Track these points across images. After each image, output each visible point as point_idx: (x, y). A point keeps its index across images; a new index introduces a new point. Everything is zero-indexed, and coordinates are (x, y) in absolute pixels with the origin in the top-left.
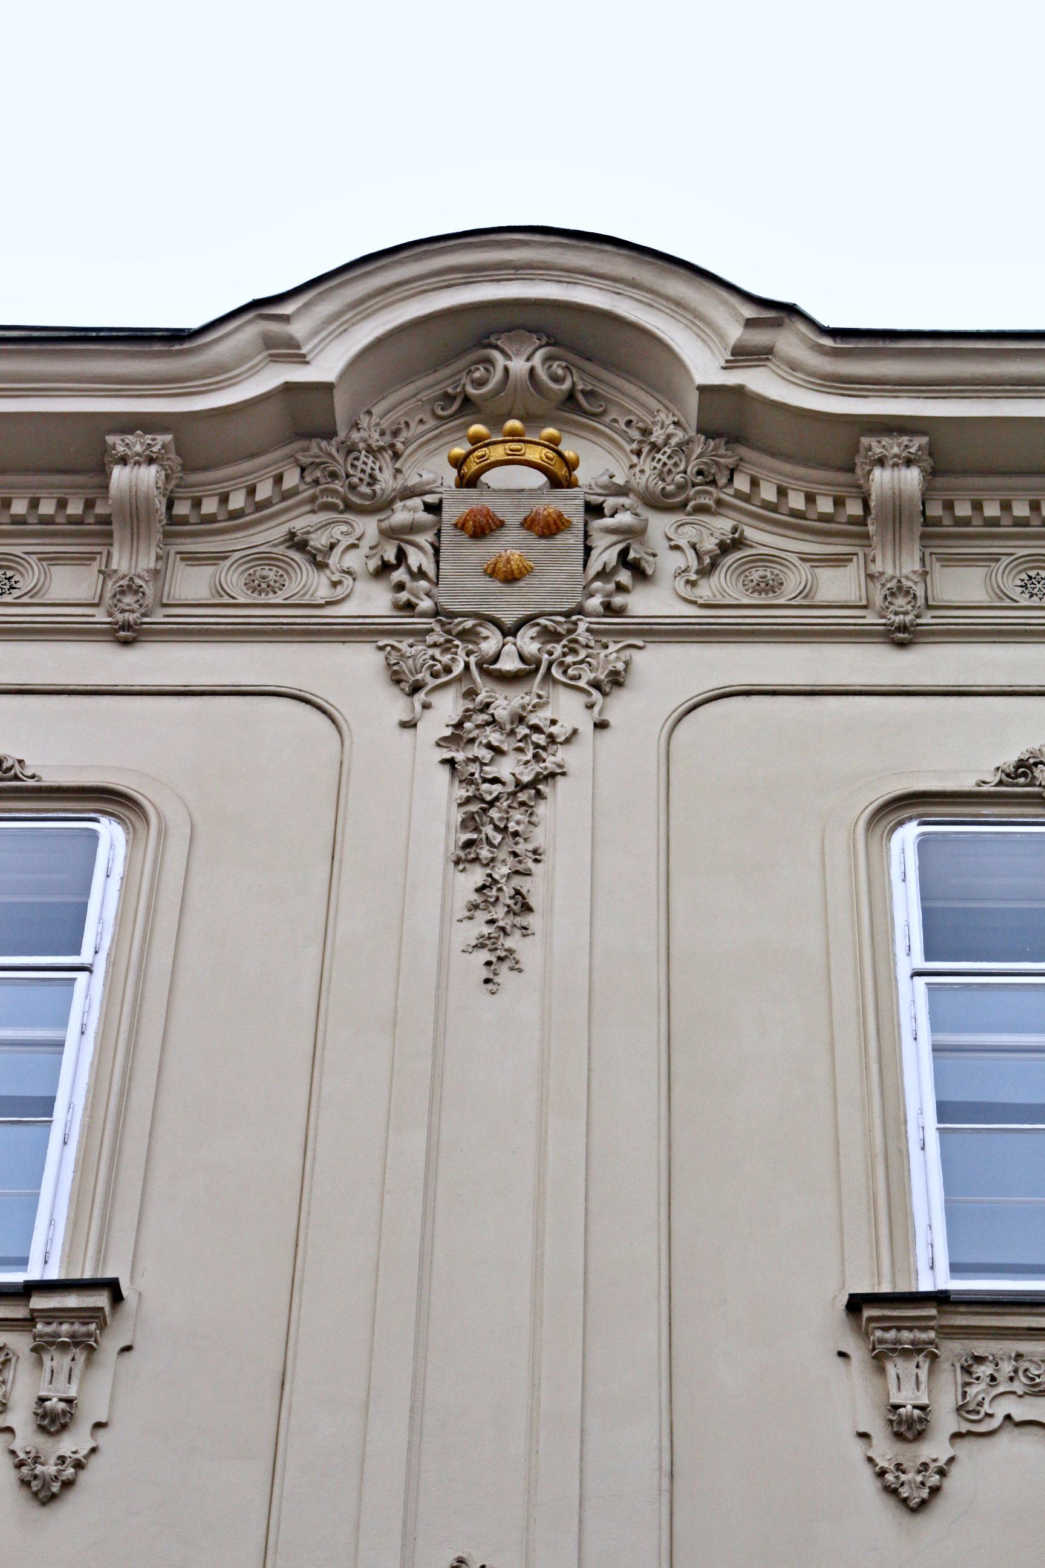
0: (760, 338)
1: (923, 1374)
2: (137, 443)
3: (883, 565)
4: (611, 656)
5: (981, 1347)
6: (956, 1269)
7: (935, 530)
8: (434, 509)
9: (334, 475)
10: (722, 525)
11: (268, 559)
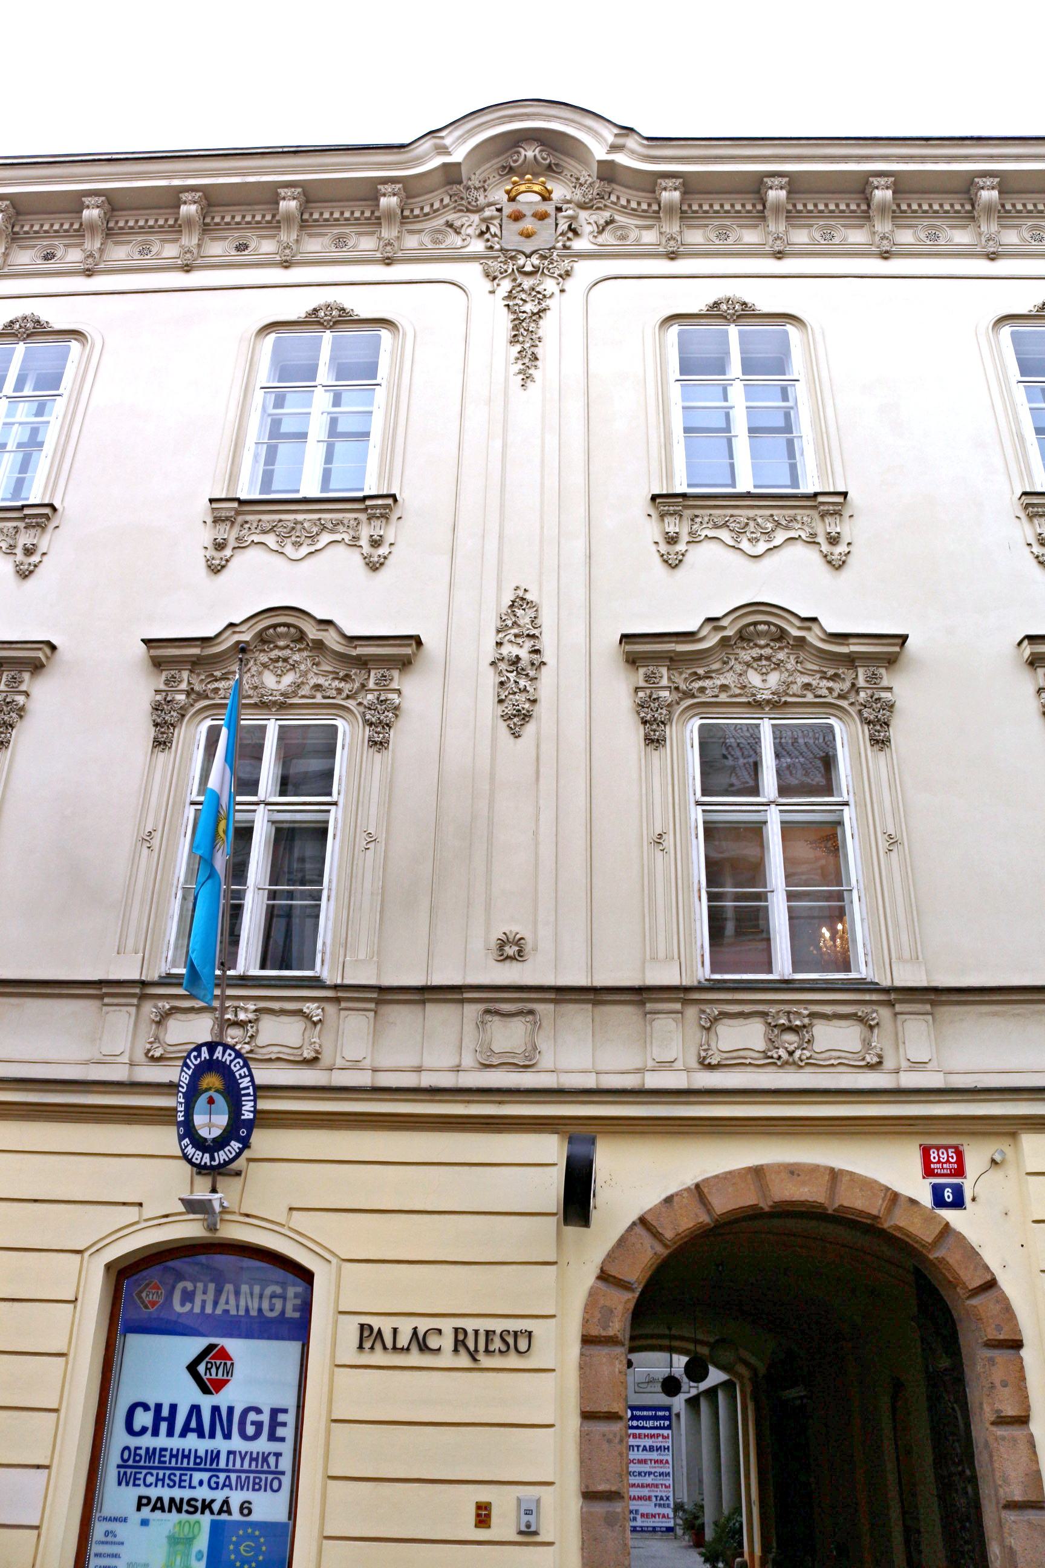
0: (620, 141)
1: (228, 528)
2: (389, 188)
3: (666, 229)
4: (566, 264)
5: (697, 512)
6: (689, 486)
7: (685, 215)
8: (500, 210)
9: (462, 199)
10: (606, 215)
11: (439, 231)
